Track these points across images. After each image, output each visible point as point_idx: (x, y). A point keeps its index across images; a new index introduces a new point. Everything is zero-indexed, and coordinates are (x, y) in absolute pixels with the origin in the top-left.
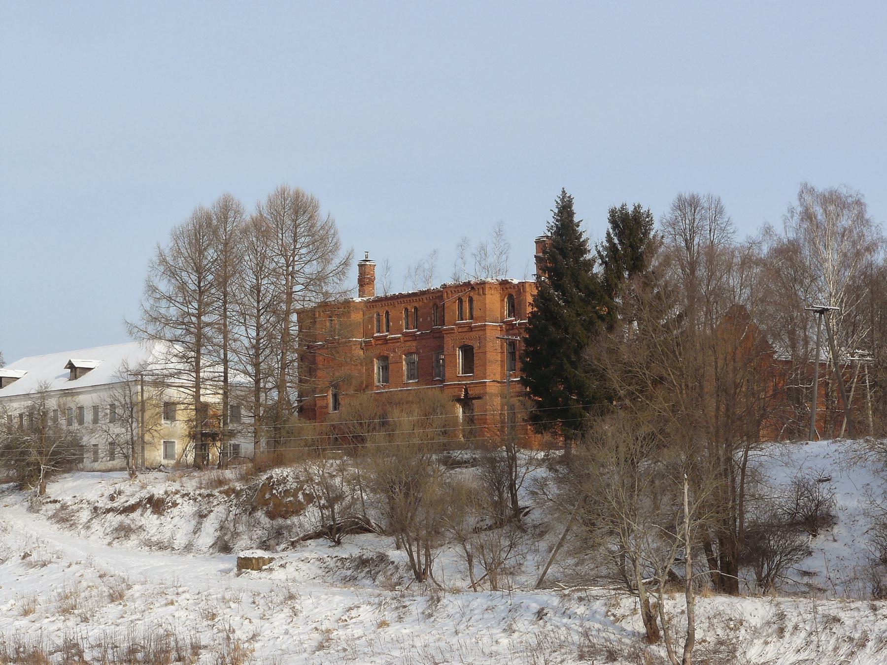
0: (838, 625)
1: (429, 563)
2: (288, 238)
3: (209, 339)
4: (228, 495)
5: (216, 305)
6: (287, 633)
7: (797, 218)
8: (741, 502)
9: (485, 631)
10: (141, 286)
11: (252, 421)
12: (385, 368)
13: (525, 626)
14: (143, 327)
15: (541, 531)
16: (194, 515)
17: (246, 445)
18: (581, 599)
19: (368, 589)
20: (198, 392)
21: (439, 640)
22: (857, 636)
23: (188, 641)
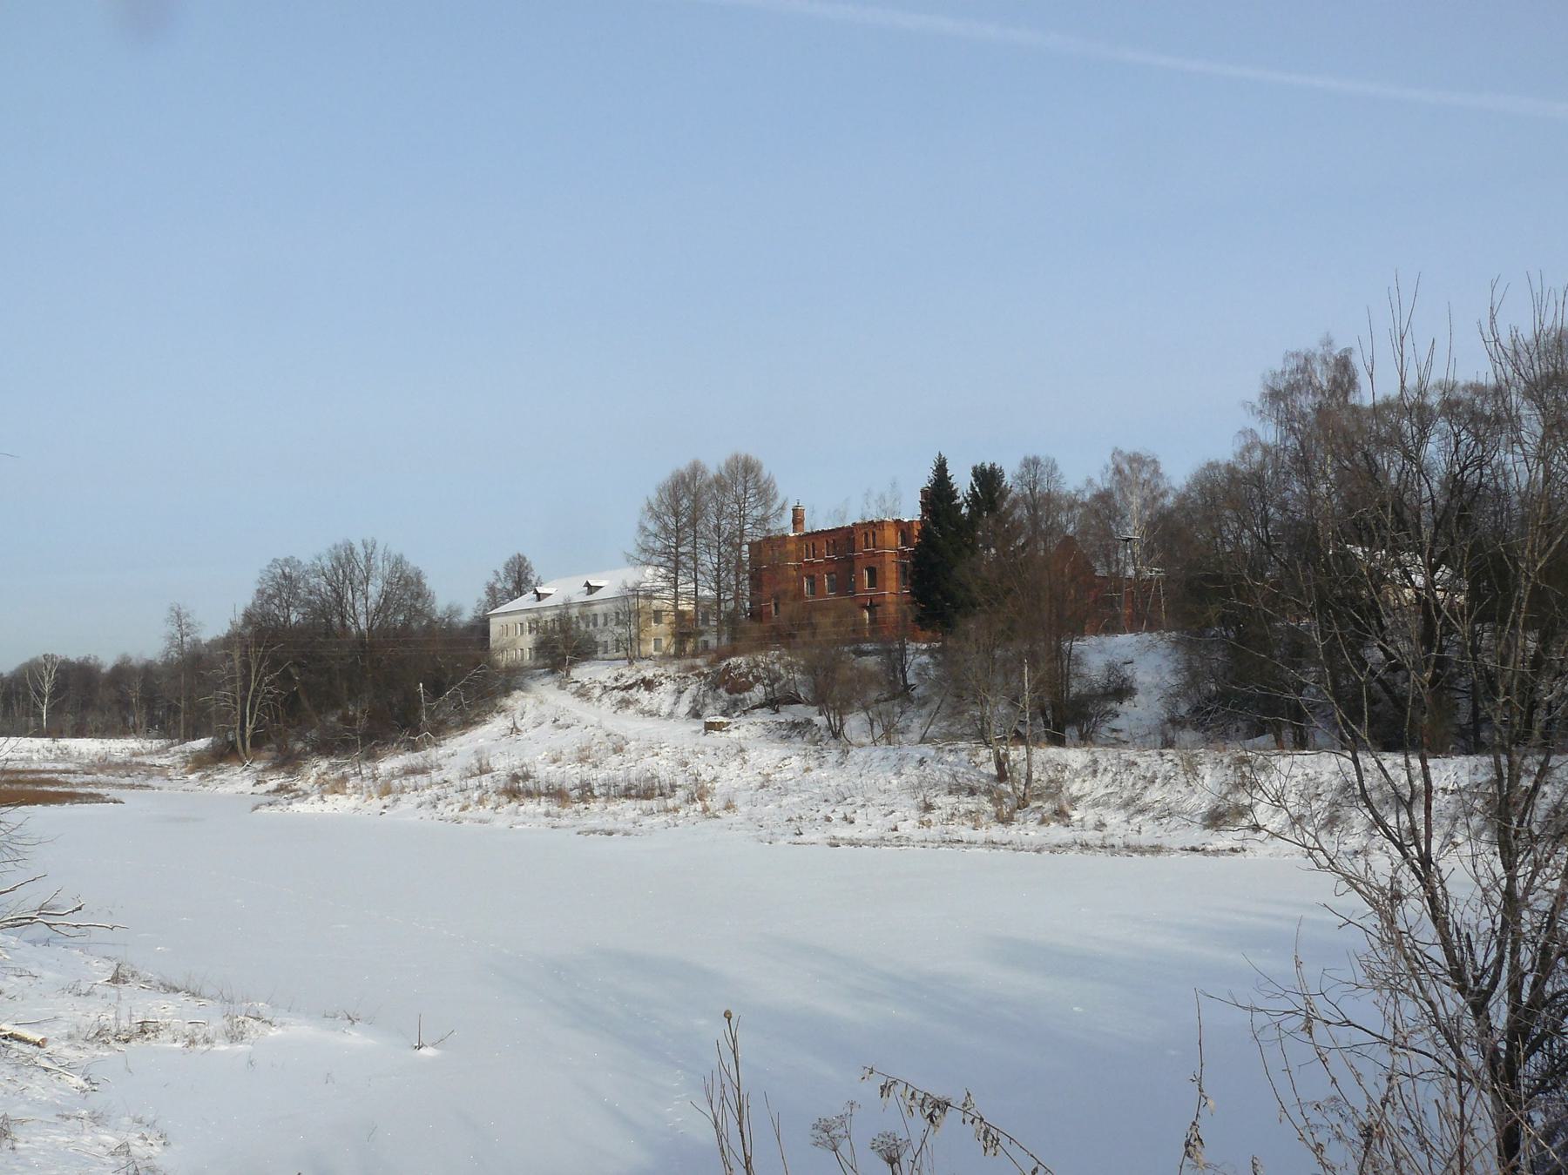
0: (1135, 767)
1: (842, 725)
2: (740, 490)
3: (684, 564)
4: (699, 678)
5: (688, 540)
6: (738, 776)
7: (1110, 472)
8: (1068, 679)
9: (881, 774)
10: (636, 526)
11: (716, 623)
12: (812, 584)
13: (910, 770)
14: (637, 556)
15: (924, 702)
16: (674, 691)
17: (713, 642)
18: (951, 751)
19: (798, 744)
20: (676, 602)
21: (848, 781)
22: (1149, 775)
23: (668, 782)
